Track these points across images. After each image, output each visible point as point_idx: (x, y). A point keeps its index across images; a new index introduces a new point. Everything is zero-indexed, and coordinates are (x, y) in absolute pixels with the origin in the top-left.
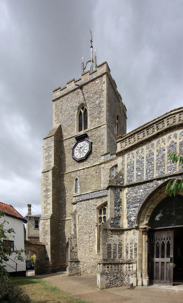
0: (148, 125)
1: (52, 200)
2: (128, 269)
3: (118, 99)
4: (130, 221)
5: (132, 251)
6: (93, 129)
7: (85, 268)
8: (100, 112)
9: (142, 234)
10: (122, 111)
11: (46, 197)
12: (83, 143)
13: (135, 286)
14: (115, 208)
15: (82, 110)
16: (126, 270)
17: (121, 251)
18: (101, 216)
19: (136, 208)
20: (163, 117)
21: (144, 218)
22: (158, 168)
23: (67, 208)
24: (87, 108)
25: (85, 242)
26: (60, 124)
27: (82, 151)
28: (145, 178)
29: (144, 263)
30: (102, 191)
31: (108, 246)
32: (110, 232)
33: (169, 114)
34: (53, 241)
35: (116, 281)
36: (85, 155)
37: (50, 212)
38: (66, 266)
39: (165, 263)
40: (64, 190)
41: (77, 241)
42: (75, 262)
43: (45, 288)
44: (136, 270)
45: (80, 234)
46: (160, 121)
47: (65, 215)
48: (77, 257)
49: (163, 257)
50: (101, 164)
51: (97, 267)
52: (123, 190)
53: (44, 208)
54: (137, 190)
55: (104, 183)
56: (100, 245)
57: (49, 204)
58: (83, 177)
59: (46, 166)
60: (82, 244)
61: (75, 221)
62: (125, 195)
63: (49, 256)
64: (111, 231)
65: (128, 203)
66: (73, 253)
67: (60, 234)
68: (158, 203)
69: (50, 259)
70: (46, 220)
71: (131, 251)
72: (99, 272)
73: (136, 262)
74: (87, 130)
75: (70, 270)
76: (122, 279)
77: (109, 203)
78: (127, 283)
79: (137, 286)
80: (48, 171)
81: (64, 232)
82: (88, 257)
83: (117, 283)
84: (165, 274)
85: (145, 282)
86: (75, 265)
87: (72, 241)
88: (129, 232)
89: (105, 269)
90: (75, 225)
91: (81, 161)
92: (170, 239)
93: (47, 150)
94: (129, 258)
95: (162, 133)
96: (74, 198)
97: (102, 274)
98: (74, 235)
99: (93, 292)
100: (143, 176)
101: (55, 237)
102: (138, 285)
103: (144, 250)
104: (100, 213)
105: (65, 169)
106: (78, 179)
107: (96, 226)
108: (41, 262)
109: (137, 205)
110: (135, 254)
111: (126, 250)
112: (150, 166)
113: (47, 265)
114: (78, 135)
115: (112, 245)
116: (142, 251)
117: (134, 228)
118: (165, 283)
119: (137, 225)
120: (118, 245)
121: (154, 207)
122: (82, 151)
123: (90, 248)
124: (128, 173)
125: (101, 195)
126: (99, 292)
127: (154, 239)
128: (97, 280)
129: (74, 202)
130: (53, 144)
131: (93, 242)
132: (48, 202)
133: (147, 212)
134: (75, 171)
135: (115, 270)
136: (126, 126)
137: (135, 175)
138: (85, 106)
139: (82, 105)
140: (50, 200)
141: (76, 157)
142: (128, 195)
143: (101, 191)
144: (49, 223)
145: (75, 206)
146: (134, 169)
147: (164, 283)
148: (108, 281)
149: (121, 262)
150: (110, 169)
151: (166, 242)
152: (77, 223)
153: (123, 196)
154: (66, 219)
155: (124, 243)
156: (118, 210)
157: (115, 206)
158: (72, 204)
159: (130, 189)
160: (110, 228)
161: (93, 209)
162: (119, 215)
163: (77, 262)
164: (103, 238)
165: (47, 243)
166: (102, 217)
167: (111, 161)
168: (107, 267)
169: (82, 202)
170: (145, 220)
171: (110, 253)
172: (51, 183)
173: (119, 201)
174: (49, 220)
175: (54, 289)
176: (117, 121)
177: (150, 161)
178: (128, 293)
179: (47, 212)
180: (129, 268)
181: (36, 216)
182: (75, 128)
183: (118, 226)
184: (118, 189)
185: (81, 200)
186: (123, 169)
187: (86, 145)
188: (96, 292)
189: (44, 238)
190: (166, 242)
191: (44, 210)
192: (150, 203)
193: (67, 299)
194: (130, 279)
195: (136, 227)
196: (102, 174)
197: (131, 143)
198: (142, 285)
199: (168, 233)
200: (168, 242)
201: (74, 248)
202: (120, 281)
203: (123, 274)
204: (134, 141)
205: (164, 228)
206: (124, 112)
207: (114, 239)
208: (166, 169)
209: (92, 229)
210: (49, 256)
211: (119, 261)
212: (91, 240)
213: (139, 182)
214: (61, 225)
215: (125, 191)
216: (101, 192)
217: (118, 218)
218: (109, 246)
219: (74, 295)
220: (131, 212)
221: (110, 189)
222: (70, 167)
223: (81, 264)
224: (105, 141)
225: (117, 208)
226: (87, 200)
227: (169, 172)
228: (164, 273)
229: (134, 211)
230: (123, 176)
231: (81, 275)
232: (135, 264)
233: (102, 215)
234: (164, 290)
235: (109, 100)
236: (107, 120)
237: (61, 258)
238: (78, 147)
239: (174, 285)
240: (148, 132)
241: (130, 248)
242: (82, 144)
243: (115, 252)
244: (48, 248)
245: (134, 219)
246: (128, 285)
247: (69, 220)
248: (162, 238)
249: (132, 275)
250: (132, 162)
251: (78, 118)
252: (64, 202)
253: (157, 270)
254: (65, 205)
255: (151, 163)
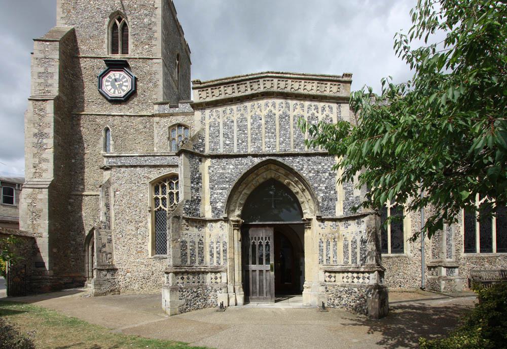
0: (240, 79)
1: (53, 154)
2: (214, 281)
3: (179, 31)
4: (216, 208)
5: (219, 254)
6: (139, 58)
7: (128, 280)
8: (151, 38)
9: (234, 229)
10: (184, 50)
11: (40, 147)
12: (120, 75)
13: (226, 307)
14: (193, 185)
15: (117, 22)
16: (212, 282)
17: (203, 253)
18: (173, 191)
19: (224, 191)
20: (260, 75)
21: (235, 207)
22: (253, 141)
23: (86, 175)
24: (128, 22)
25: (129, 237)
26: (72, 27)
27: (118, 86)
28: (235, 151)
29: (238, 272)
30: (159, 157)
31: (181, 244)
32: (184, 221)
33: (266, 75)
34: (55, 230)
35: (195, 300)
36: (123, 94)
37: (49, 176)
38: (86, 278)
39: (264, 272)
40: (80, 141)
41: (113, 233)
42: (108, 270)
43: (48, 322)
44: (226, 282)
45: (117, 221)
46: (255, 79)
47: (82, 187)
48: (112, 262)
49: (261, 263)
50: (153, 116)
51: (152, 279)
52: (203, 160)
53: (32, 166)
54: (225, 164)
55: (159, 147)
56: (168, 242)
57: (46, 160)
58: (120, 128)
59: (40, 90)
60: (122, 240)
61: (107, 199)
62: (207, 168)
63: (46, 259)
64: (186, 221)
65: (211, 181)
66: (104, 254)
67: (71, 219)
68: (253, 187)
69: (47, 265)
70: (38, 190)
71: (219, 253)
72: (166, 286)
73: (227, 270)
74: (127, 56)
75: (97, 285)
76: (205, 297)
77: (182, 176)
78: (214, 302)
79: (229, 306)
80: (44, 100)
81: (81, 217)
82: (134, 262)
83: (197, 304)
84: (264, 287)
85: (240, 299)
86: (109, 276)
87: (101, 233)
88: (214, 224)
89: (177, 281)
90: (107, 206)
91: (115, 101)
92: (269, 239)
93: (44, 60)
94: (215, 264)
95: (258, 96)
96: (105, 159)
97: (173, 290)
98: (104, 223)
99: (159, 321)
100: (233, 146)
101: (60, 224)
102: (230, 305)
103: (236, 253)
104: (156, 192)
105: (83, 107)
106: (111, 130)
107: (150, 211)
108: (24, 271)
109: (225, 186)
110: (225, 258)
111: (211, 251)
112: (243, 135)
113: (40, 277)
114: (110, 58)
115: (188, 243)
116: (234, 253)
117: (221, 220)
118: (265, 299)
119: (226, 216)
120: (197, 244)
121: (249, 193)
122: (118, 86)
123: (139, 246)
124: (210, 138)
125: (158, 164)
126: (170, 319)
127: (249, 237)
128: (163, 300)
129: (105, 166)
130: (57, 57)
131: (144, 237)
132: (44, 156)
133: (240, 197)
134: (105, 115)
135: (194, 282)
136: (190, 74)
137: (221, 143)
138: (123, 17)
139: (118, 14)
140: (49, 154)
141: (106, 92)
142: (212, 169)
143: (157, 157)
144: (47, 197)
145: (107, 174)
146: (219, 133)
147: (264, 299)
148: (184, 301)
149: (202, 270)
150: (169, 127)
151: (264, 243)
152: (112, 202)
153: (203, 170)
154: (85, 193)
155: (207, 241)
156: (197, 190)
157: (192, 182)
158: (102, 168)
159: (214, 161)
160: (184, 215)
161: (142, 182)
162: (197, 197)
163: (113, 270)
164: (172, 230)
165: (42, 233)
166: (160, 198)
167: (171, 116)
168: (181, 278)
169: (123, 169)
170: (237, 210)
171: (186, 255)
172: (52, 124)
173: (197, 175)
174: (46, 192)
175: (73, 322)
176: (177, 62)
177: (242, 129)
178: (218, 319)
179: (41, 176)
180: (216, 279)
181: (6, 180)
182: (105, 46)
183: (197, 215)
184: (197, 157)
185: (119, 164)
186: (203, 129)
187: (126, 79)
188: (164, 321)
189: (33, 224)
190: (264, 243)
191: (34, 170)
192: (244, 187)
193: (113, 339)
194: (218, 296)
195: (224, 218)
196: (156, 132)
197: (214, 95)
198: (236, 305)
199: (266, 230)
200: (267, 242)
201: (105, 245)
202: (202, 301)
203: (206, 289)
204: (220, 94)
205: (261, 223)
206: (187, 53)
207: (191, 233)
208: (264, 144)
209: (142, 216)
210: (46, 259)
211: (200, 269)
212: (140, 234)
213: (228, 153)
214: (73, 203)
215: (206, 163)
216: (158, 159)
217: (197, 201)
218: (184, 244)
219: (123, 330)
220: (216, 196)
221: (183, 155)
222: (92, 106)
223: (120, 273)
224: (161, 83)
225: (195, 186)
226: (132, 166)
227: (267, 149)
228: (263, 285)
229: (221, 194)
230: (203, 140)
231: (119, 294)
232: (225, 274)
233: (160, 195)
234: (268, 310)
235: (165, 26)
236: (163, 53)
237: (74, 263)
238: (110, 77)
239: (276, 301)
240: (238, 88)
241: (217, 248)
242: (118, 75)
243: (193, 255)
244: (43, 244)
245: (221, 207)
246: (214, 306)
247: (91, 195)
248: (259, 238)
249: (221, 289)
250: (217, 123)
251: (110, 32)
252: (81, 164)
253: (254, 283)
254: (83, 168)
255: (244, 131)
